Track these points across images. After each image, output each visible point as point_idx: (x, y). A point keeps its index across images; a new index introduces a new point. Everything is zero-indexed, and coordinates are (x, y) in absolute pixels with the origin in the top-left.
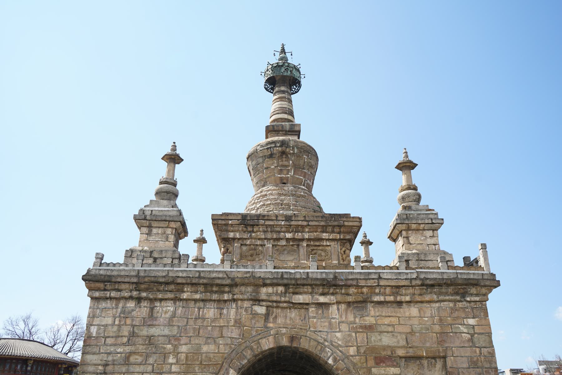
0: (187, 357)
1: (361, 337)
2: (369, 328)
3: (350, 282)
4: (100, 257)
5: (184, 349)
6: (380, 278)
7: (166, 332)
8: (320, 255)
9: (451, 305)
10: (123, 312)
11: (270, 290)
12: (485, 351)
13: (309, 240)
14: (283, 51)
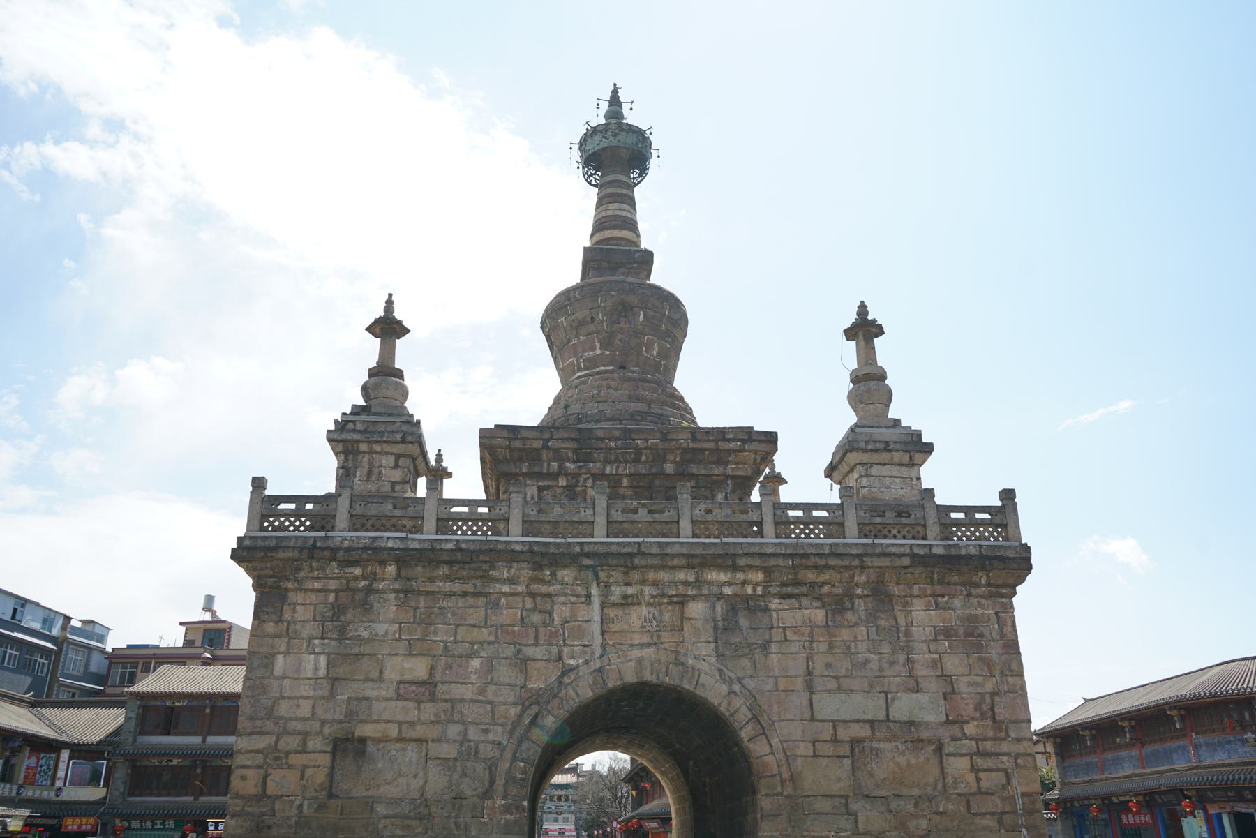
14: (615, 100)
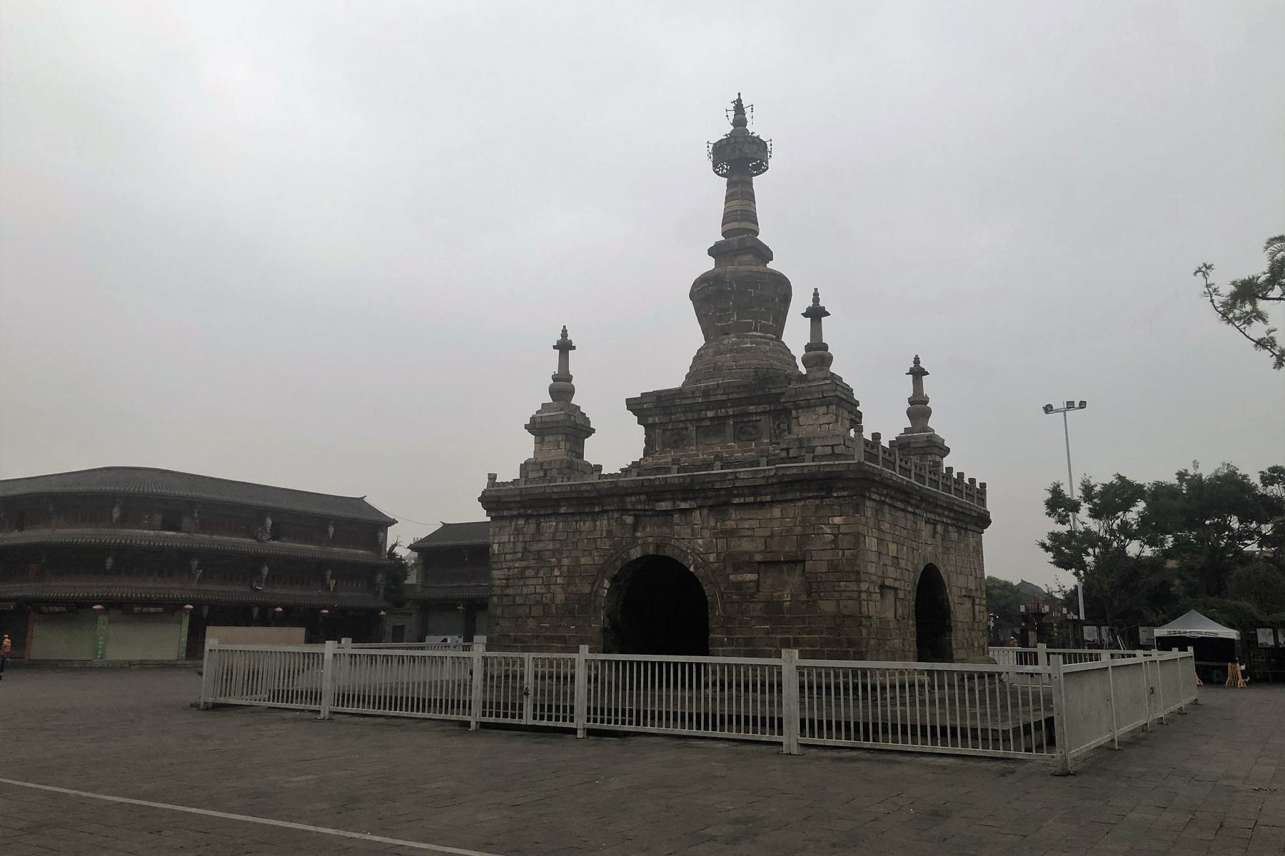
0: (568, 570)
1: (722, 543)
2: (731, 533)
3: (705, 486)
4: (492, 477)
5: (565, 561)
6: (737, 478)
7: (551, 547)
8: (750, 434)
9: (818, 502)
10: (516, 529)
11: (633, 499)
12: (848, 553)
13: (734, 416)
14: (739, 107)
